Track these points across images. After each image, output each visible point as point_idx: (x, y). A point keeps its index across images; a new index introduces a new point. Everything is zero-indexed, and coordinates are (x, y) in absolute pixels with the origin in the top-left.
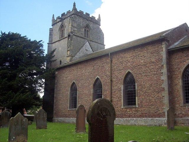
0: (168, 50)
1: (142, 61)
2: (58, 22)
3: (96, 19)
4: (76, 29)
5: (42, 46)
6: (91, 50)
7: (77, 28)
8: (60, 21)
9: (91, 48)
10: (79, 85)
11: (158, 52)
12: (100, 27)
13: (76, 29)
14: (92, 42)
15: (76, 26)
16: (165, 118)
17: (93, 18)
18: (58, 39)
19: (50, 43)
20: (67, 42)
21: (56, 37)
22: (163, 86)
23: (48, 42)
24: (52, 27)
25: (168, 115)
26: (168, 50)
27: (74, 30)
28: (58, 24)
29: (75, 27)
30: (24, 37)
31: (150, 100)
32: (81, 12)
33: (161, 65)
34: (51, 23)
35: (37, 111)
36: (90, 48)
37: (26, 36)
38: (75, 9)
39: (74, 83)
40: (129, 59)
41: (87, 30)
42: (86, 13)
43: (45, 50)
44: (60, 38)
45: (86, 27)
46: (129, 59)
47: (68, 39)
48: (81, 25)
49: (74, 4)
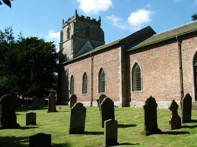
1: (109, 60)
2: (66, 26)
3: (97, 20)
4: (77, 32)
5: (54, 46)
7: (79, 31)
8: (68, 25)
10: (75, 77)
11: (117, 53)
12: (101, 27)
13: (77, 32)
14: (92, 41)
16: (119, 102)
17: (94, 20)
18: (67, 40)
19: (61, 44)
21: (65, 38)
22: (119, 79)
27: (76, 32)
29: (77, 30)
30: (41, 39)
31: (112, 88)
32: (83, 17)
33: (118, 63)
34: (62, 26)
35: (26, 98)
37: (42, 39)
38: (77, 15)
39: (102, 69)
40: (102, 58)
41: (88, 30)
42: (88, 17)
45: (87, 29)
46: (102, 58)
47: (72, 40)
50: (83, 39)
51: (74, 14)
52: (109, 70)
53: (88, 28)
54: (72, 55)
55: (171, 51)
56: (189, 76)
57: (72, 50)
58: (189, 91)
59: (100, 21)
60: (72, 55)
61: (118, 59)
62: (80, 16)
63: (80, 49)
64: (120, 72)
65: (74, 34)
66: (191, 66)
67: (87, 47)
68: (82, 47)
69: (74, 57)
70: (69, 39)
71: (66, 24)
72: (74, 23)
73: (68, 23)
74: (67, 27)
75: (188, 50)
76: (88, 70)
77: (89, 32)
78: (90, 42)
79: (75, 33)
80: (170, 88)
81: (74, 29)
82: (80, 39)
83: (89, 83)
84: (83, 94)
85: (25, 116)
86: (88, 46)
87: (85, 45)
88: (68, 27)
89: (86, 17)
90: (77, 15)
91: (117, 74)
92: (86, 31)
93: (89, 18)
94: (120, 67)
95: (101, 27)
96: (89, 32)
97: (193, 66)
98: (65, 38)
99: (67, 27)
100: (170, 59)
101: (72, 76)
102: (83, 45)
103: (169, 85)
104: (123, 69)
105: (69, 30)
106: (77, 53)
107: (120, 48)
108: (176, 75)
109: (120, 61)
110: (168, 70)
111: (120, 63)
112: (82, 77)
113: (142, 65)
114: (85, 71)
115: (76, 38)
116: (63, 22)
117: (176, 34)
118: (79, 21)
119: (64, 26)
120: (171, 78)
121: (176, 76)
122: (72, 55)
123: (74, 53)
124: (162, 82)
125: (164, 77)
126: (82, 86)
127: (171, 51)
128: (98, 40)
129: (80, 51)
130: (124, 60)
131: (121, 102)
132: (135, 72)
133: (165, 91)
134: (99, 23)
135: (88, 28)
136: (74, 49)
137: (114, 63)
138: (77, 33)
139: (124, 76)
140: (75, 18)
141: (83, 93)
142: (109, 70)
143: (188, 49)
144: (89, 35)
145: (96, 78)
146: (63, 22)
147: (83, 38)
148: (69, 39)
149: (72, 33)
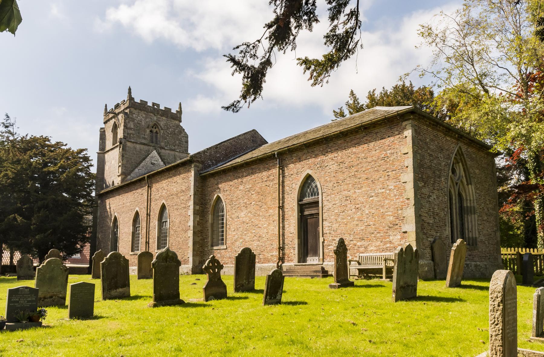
0: (201, 175)
1: (175, 189)
2: (111, 118)
3: (174, 111)
6: (162, 163)
7: (134, 130)
8: (113, 117)
9: (162, 161)
12: (181, 124)
14: (163, 151)
15: (132, 126)
16: (187, 266)
17: (168, 110)
18: (112, 147)
20: (118, 151)
23: (98, 151)
24: (103, 126)
25: (103, 276)
26: (201, 175)
27: (128, 134)
28: (111, 121)
34: (102, 119)
36: (160, 160)
38: (131, 99)
41: (154, 130)
42: (154, 104)
43: (92, 160)
44: (113, 144)
47: (120, 148)
48: (143, 123)
49: (130, 89)
50: (142, 147)
51: (126, 98)
52: (175, 207)
53: (156, 126)
54: (120, 177)
55: (268, 177)
56: (291, 221)
57: (120, 168)
58: (290, 246)
59: (180, 112)
60: (120, 178)
61: (188, 189)
62: (137, 100)
63: (136, 167)
64: (191, 212)
65: (125, 137)
66: (294, 204)
67: (152, 164)
68: (141, 162)
69: (122, 181)
70: (116, 145)
71: (111, 115)
72: (126, 114)
73: (115, 113)
74: (112, 122)
75: (292, 176)
76: (141, 207)
77: (157, 133)
78: (159, 154)
79: (126, 135)
80: (265, 242)
81: (124, 126)
82: (138, 146)
83: (143, 232)
84: (132, 253)
85: (6, 296)
86: (153, 161)
87: (148, 159)
88: (115, 122)
89: (150, 104)
90: (131, 99)
91: (187, 216)
92: (151, 131)
93: (158, 105)
94: (191, 203)
95: (181, 124)
96: (157, 133)
97: (298, 204)
98: (109, 144)
99: (112, 122)
100: (267, 192)
101: (163, 208)
102: (144, 159)
103: (264, 236)
104: (197, 207)
105: (115, 127)
106: (129, 174)
107: (408, 133)
108: (274, 220)
109: (192, 192)
110: (263, 209)
111: (192, 197)
112: (132, 221)
113: (227, 201)
114: (137, 209)
115: (129, 144)
116: (106, 109)
117: (276, 149)
118: (135, 112)
119: (107, 119)
120: (268, 223)
121: (274, 221)
122: (120, 177)
123: (123, 174)
124: (254, 231)
125: (257, 222)
126: (131, 237)
127: (268, 177)
128: (174, 150)
129: (136, 170)
130: (200, 190)
131: (190, 266)
132: (309, 197)
133: (258, 245)
134: (177, 117)
135: (156, 126)
136: (123, 166)
137: (183, 196)
138: (131, 134)
139: (198, 219)
140: (127, 105)
141: (132, 251)
142: (175, 207)
143: (292, 175)
144: (157, 138)
145: (154, 223)
146: (106, 109)
147: (144, 144)
148: (116, 145)
149: (120, 134)
